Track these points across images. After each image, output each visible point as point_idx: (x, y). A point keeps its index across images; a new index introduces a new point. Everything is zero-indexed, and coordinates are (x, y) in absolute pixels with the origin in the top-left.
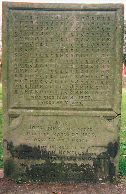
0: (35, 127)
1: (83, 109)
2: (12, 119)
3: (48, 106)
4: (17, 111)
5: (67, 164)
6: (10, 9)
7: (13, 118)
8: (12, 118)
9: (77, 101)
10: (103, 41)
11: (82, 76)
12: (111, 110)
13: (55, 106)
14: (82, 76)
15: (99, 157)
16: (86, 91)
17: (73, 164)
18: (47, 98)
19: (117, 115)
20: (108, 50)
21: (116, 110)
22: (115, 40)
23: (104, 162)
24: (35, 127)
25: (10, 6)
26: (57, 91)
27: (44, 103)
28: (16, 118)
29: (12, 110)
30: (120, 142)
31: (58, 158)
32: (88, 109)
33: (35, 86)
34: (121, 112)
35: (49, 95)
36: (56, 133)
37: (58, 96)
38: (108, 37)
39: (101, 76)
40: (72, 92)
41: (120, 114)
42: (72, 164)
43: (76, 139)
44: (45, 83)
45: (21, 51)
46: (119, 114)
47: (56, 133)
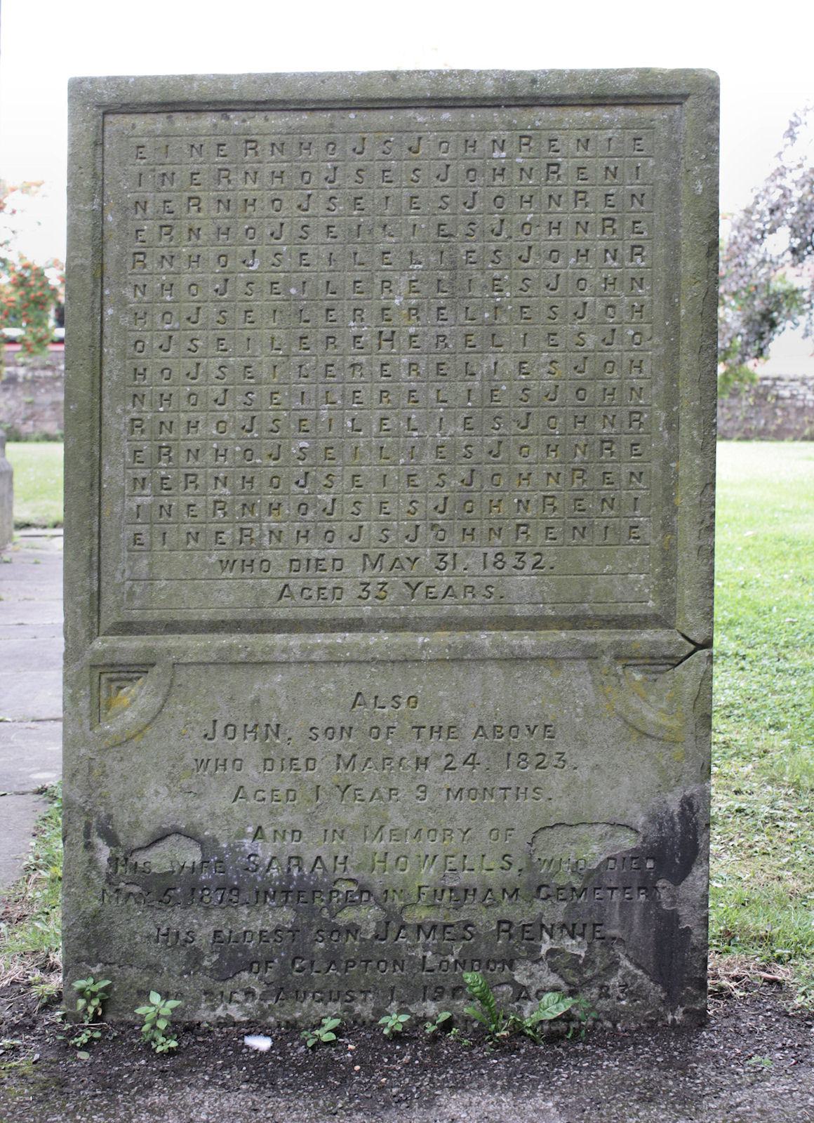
0: (240, 730)
1: (510, 623)
2: (114, 686)
3: (309, 612)
4: (133, 644)
5: (420, 927)
6: (108, 110)
7: (118, 684)
8: (111, 680)
9: (472, 581)
10: (610, 262)
11: (500, 442)
12: (661, 621)
13: (345, 609)
14: (500, 442)
15: (594, 880)
16: (519, 525)
17: (451, 926)
18: (304, 567)
19: (692, 647)
20: (469, 531)
21: (688, 619)
22: (672, 424)
23: (622, 905)
24: (240, 730)
25: (108, 96)
26: (361, 527)
27: (291, 596)
28: (138, 678)
29: (113, 640)
30: (721, 803)
31: (365, 897)
32: (534, 623)
33: (238, 507)
34: (711, 631)
35: (315, 553)
36: (354, 756)
37: (366, 555)
38: (635, 243)
39: (603, 442)
40: (441, 534)
41: (708, 644)
42: (445, 926)
43: (467, 786)
44: (295, 488)
45: (167, 326)
46: (699, 641)
47: (354, 756)
